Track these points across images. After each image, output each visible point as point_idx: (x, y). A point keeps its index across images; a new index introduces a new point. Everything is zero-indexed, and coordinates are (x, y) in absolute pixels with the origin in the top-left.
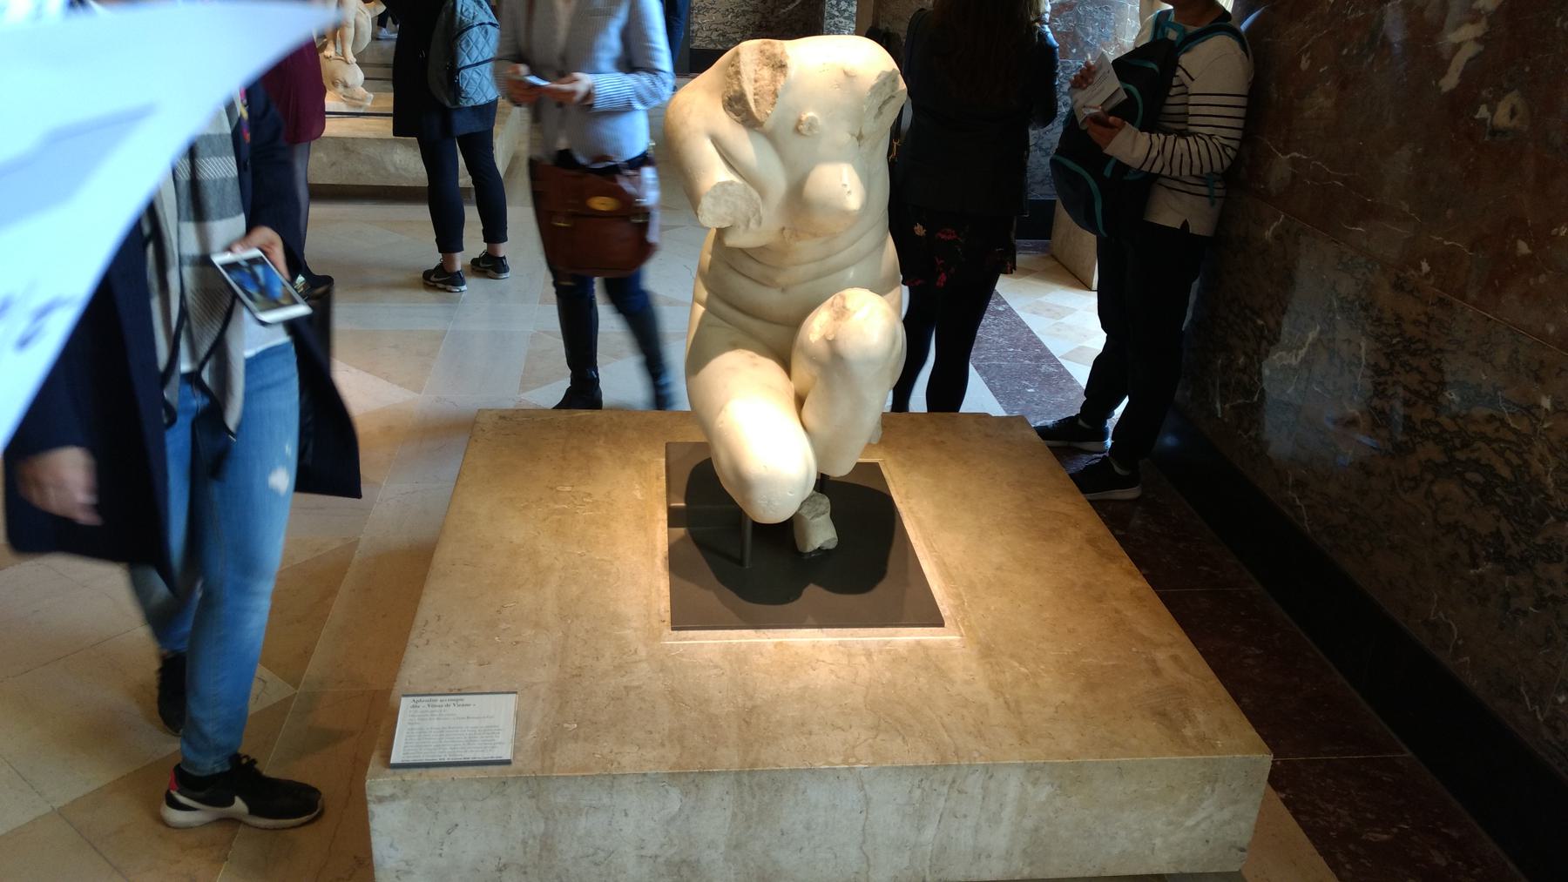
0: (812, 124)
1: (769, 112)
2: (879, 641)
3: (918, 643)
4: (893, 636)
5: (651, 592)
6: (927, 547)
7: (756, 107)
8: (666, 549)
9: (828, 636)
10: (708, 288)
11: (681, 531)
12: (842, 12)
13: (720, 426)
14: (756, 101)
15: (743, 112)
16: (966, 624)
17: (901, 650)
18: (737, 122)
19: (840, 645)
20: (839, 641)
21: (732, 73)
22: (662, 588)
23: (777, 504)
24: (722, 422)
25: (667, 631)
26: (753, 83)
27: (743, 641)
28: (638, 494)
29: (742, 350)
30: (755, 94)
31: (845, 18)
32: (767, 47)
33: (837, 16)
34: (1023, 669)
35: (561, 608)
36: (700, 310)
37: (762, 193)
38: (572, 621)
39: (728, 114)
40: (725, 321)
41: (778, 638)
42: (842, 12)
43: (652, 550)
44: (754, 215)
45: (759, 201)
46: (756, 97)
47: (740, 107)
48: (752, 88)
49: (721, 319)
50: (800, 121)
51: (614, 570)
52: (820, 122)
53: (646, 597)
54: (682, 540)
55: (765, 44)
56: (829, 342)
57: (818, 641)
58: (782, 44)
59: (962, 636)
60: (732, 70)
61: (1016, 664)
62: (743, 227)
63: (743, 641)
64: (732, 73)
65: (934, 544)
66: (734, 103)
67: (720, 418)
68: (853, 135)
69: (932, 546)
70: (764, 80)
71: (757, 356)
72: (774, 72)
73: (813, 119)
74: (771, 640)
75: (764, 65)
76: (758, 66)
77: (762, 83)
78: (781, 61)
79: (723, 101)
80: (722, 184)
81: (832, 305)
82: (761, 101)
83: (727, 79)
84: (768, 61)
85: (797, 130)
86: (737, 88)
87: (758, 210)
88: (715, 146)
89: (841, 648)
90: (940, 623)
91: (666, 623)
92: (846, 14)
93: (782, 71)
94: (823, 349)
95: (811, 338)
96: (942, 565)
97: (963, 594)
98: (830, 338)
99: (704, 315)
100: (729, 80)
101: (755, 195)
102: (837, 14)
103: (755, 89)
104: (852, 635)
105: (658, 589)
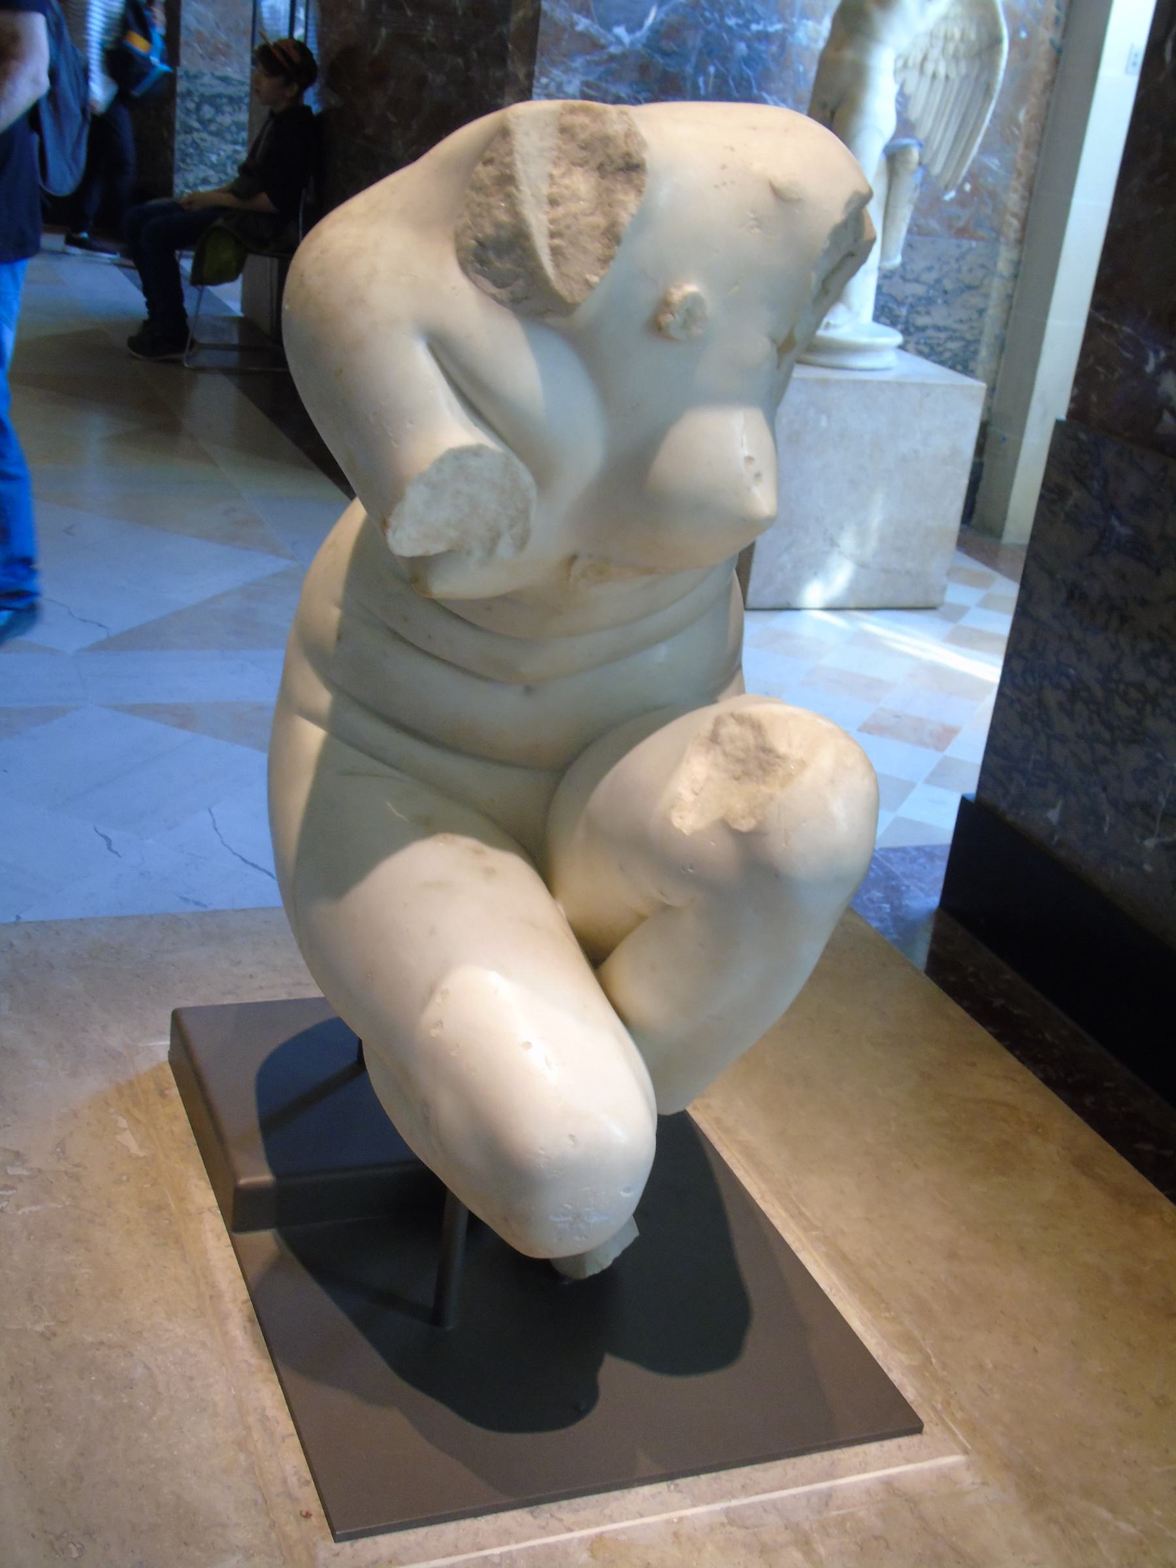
0: (692, 310)
1: (594, 279)
2: (808, 1496)
3: (888, 1485)
4: (830, 1476)
5: (248, 1428)
6: (792, 1217)
7: (557, 265)
8: (245, 1295)
9: (696, 1502)
11: (265, 1240)
12: (205, 123)
13: (434, 1032)
14: (555, 252)
16: (959, 1415)
17: (862, 1513)
18: (500, 302)
19: (732, 1522)
20: (727, 1512)
21: (488, 182)
22: (270, 1413)
23: (594, 1220)
25: (327, 1547)
26: (547, 208)
27: (513, 1547)
28: (130, 1141)
29: (450, 837)
30: (552, 235)
31: (211, 133)
32: (580, 119)
33: (197, 130)
34: (1124, 1526)
35: (41, 1512)
36: (313, 736)
37: (543, 475)
38: (82, 1550)
39: (474, 282)
40: (384, 761)
41: (588, 1525)
42: (205, 123)
44: (511, 526)
45: (533, 494)
46: (557, 242)
47: (509, 266)
48: (544, 218)
49: (373, 756)
50: (665, 305)
51: (140, 1371)
52: (711, 307)
53: (241, 1445)
54: (276, 1266)
55: (573, 111)
56: (738, 835)
57: (681, 1519)
58: (622, 113)
59: (965, 1452)
60: (485, 173)
61: (1105, 1514)
62: (478, 553)
63: (513, 1547)
64: (488, 182)
65: (804, 1209)
66: (491, 255)
67: (432, 1013)
68: (774, 341)
69: (801, 1214)
71: (488, 850)
72: (605, 183)
73: (695, 300)
74: (577, 1534)
75: (574, 164)
76: (556, 164)
77: (574, 207)
78: (628, 155)
80: (459, 455)
81: (714, 739)
82: (570, 251)
83: (473, 194)
84: (584, 154)
85: (656, 328)
86: (504, 218)
87: (524, 514)
88: (438, 360)
89: (739, 1533)
90: (914, 1427)
91: (314, 1520)
92: (213, 128)
93: (629, 181)
94: (720, 851)
95: (677, 822)
96: (839, 1259)
97: (917, 1333)
98: (746, 825)
99: (327, 746)
100: (481, 198)
101: (527, 479)
102: (196, 125)
103: (552, 222)
104: (745, 1489)
105: (264, 1419)
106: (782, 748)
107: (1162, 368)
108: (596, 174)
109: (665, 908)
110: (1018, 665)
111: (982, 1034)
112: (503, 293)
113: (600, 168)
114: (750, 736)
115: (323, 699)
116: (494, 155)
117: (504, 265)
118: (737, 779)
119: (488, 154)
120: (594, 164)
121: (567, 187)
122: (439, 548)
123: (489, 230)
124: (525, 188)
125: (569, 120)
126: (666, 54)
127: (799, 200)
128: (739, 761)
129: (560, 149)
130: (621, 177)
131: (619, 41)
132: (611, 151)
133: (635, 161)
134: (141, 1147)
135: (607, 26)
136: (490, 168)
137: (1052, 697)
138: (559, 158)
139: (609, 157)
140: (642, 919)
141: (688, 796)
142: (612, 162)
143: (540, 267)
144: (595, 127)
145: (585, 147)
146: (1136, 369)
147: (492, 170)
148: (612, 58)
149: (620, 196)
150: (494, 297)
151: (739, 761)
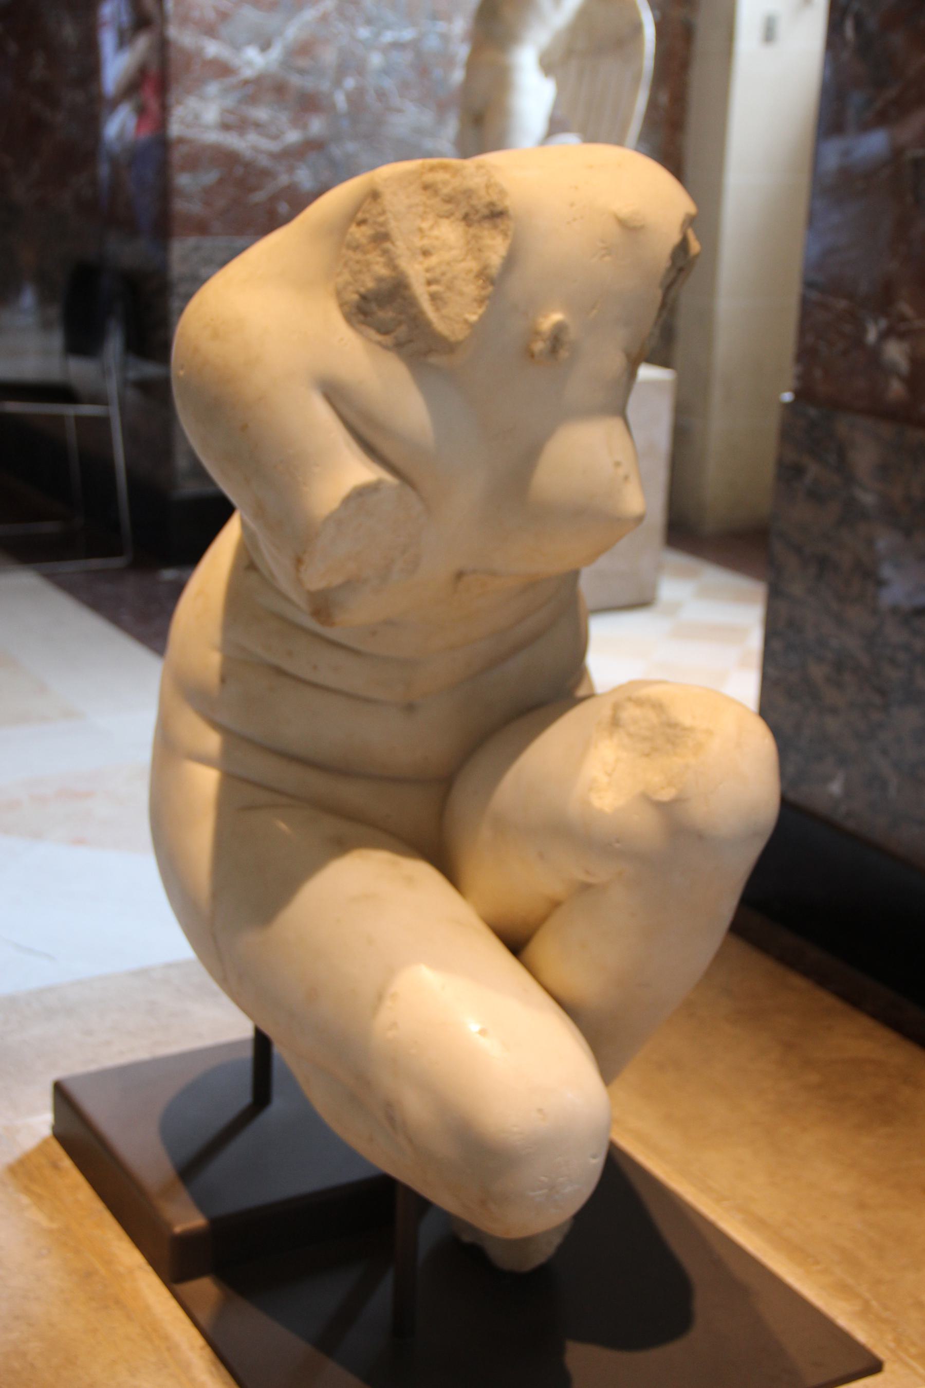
7: (437, 309)
10: (216, 726)
13: (390, 1034)
14: (434, 297)
15: (400, 323)
16: (913, 1350)
18: (385, 347)
21: (364, 241)
23: (568, 1189)
24: (394, 1025)
32: (440, 176)
39: (360, 332)
43: (169, 1349)
46: (434, 288)
56: (661, 807)
64: (364, 241)
66: (374, 306)
70: (451, 248)
72: (472, 231)
75: (440, 216)
77: (447, 256)
79: (342, 305)
80: (361, 493)
83: (350, 253)
93: (495, 227)
96: (758, 1224)
98: (666, 795)
100: (358, 256)
106: (686, 720)
107: (884, 336)
108: (463, 224)
109: (586, 887)
110: (777, 645)
111: (828, 1000)
112: (388, 340)
113: (466, 218)
114: (652, 716)
115: (212, 741)
116: (367, 216)
117: (386, 314)
118: (647, 755)
119: (360, 216)
120: (459, 214)
121: (437, 238)
122: (337, 580)
123: (370, 284)
124: (400, 243)
125: (429, 177)
126: (302, 72)
127: (642, 227)
128: (645, 739)
129: (425, 205)
130: (486, 224)
131: (249, 63)
132: (474, 202)
133: (499, 208)
134: (51, 1219)
135: (237, 47)
136: (364, 228)
137: (818, 672)
138: (425, 212)
139: (473, 207)
140: (556, 904)
141: (603, 779)
142: (477, 212)
143: (422, 313)
144: (456, 182)
145: (449, 200)
146: (858, 341)
147: (367, 230)
148: (246, 82)
149: (488, 241)
150: (379, 343)
151: (645, 739)
